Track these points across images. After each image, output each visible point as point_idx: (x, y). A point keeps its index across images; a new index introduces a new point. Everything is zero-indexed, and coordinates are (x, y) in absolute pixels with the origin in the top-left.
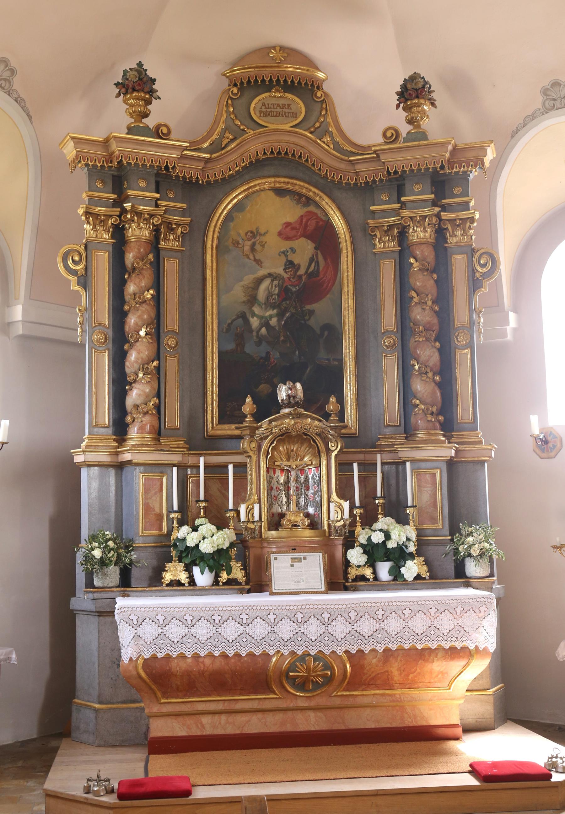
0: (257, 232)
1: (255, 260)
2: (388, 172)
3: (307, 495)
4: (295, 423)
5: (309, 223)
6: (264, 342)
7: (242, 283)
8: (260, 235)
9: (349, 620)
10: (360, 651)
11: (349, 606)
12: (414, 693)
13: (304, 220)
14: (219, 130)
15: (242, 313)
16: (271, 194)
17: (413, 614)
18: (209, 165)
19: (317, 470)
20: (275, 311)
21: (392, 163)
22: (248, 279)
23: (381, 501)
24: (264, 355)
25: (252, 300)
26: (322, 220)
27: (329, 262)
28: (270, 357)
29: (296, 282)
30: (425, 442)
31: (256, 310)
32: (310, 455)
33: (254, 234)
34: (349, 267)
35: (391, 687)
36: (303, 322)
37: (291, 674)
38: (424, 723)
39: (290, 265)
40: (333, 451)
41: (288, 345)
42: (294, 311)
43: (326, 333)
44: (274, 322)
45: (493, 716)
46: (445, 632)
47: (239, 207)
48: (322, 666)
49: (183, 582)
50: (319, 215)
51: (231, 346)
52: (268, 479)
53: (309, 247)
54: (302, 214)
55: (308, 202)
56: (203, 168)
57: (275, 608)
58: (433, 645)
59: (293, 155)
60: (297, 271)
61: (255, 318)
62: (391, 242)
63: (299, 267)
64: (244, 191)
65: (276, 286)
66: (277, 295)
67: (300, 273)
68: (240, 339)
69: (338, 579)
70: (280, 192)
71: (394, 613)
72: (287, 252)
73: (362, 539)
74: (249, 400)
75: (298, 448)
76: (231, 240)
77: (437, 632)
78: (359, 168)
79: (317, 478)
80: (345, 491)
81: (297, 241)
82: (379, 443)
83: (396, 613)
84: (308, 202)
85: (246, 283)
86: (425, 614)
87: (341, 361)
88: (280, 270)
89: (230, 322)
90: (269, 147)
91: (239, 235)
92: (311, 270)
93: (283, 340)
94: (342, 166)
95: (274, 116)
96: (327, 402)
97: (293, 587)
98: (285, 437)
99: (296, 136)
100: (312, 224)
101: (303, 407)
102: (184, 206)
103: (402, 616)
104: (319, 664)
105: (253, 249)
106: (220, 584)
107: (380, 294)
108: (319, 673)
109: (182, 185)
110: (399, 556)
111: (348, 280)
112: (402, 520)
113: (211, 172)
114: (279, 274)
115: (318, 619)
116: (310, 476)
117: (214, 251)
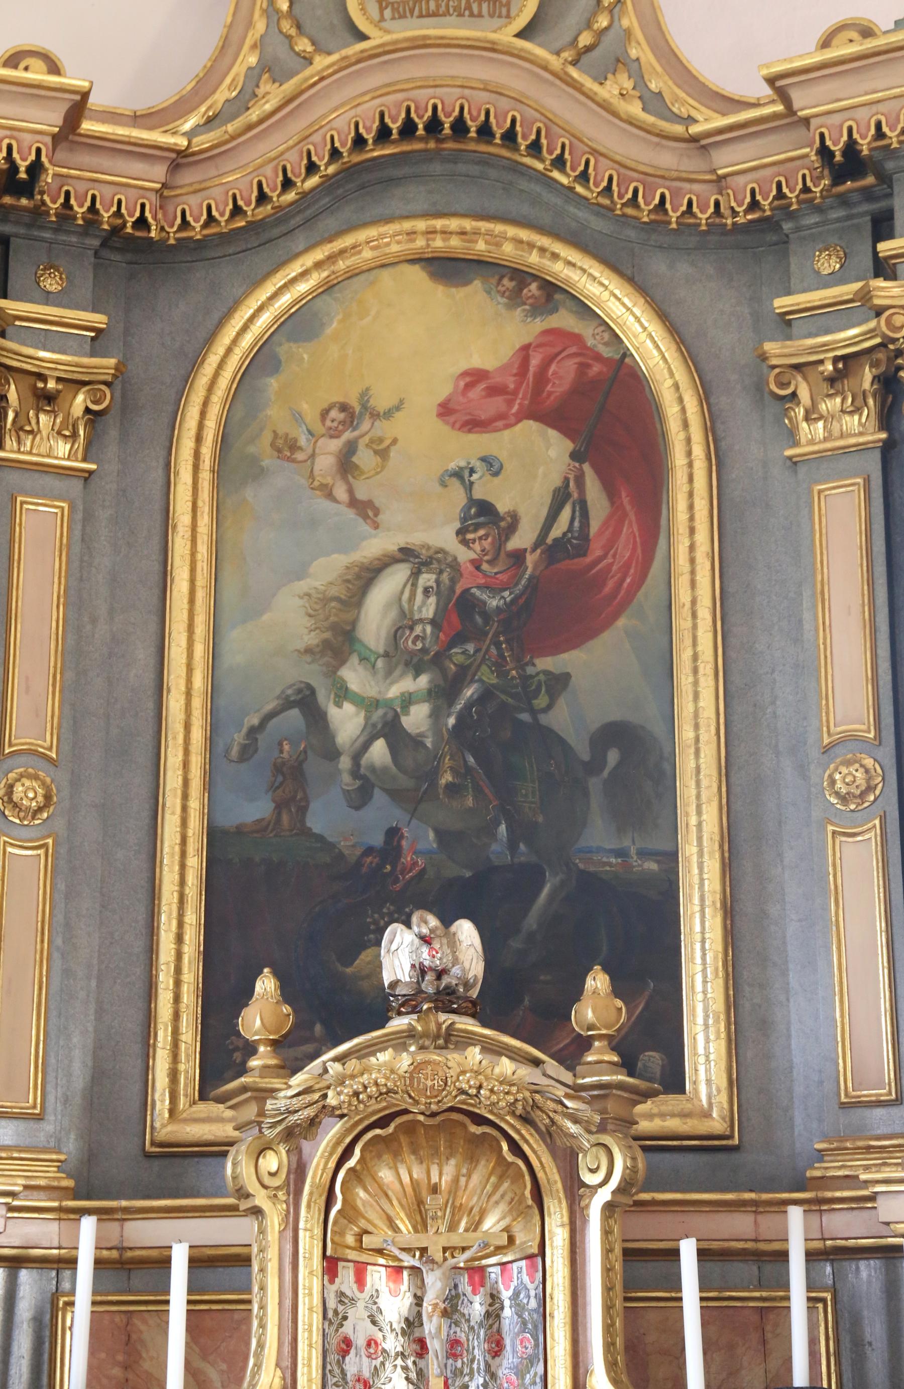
0: (364, 406)
1: (354, 502)
2: (824, 152)
3: (493, 1376)
4: (417, 1067)
5: (553, 367)
6: (377, 792)
7: (303, 586)
8: (375, 416)
13: (535, 362)
14: (239, 70)
15: (300, 691)
16: (416, 274)
18: (188, 177)
20: (424, 681)
21: (836, 119)
22: (327, 571)
24: (377, 840)
25: (340, 642)
26: (598, 357)
27: (626, 500)
28: (399, 848)
29: (503, 577)
31: (354, 676)
32: (503, 1207)
34: (697, 516)
36: (525, 717)
39: (481, 515)
40: (594, 1189)
41: (470, 802)
42: (492, 679)
43: (613, 757)
44: (417, 719)
47: (299, 324)
50: (590, 342)
51: (256, 809)
53: (552, 453)
54: (526, 340)
55: (549, 298)
56: (164, 186)
60: (507, 539)
61: (348, 707)
62: (851, 413)
63: (513, 524)
64: (318, 265)
65: (426, 591)
66: (433, 622)
67: (514, 544)
68: (291, 782)
70: (448, 268)
72: (472, 471)
75: (456, 1180)
76: (267, 437)
78: (728, 160)
79: (533, 1304)
81: (507, 433)
82: (818, 1173)
84: (549, 298)
85: (317, 584)
87: (670, 858)
88: (444, 537)
89: (255, 721)
90: (398, 105)
91: (298, 417)
92: (557, 532)
93: (449, 787)
95: (429, 15)
96: (576, 993)
98: (389, 1128)
99: (492, 60)
100: (564, 374)
101: (474, 1010)
102: (99, 319)
105: (346, 465)
107: (815, 606)
109: (96, 254)
111: (692, 561)
113: (194, 200)
114: (440, 551)
116: (506, 1295)
117: (205, 476)
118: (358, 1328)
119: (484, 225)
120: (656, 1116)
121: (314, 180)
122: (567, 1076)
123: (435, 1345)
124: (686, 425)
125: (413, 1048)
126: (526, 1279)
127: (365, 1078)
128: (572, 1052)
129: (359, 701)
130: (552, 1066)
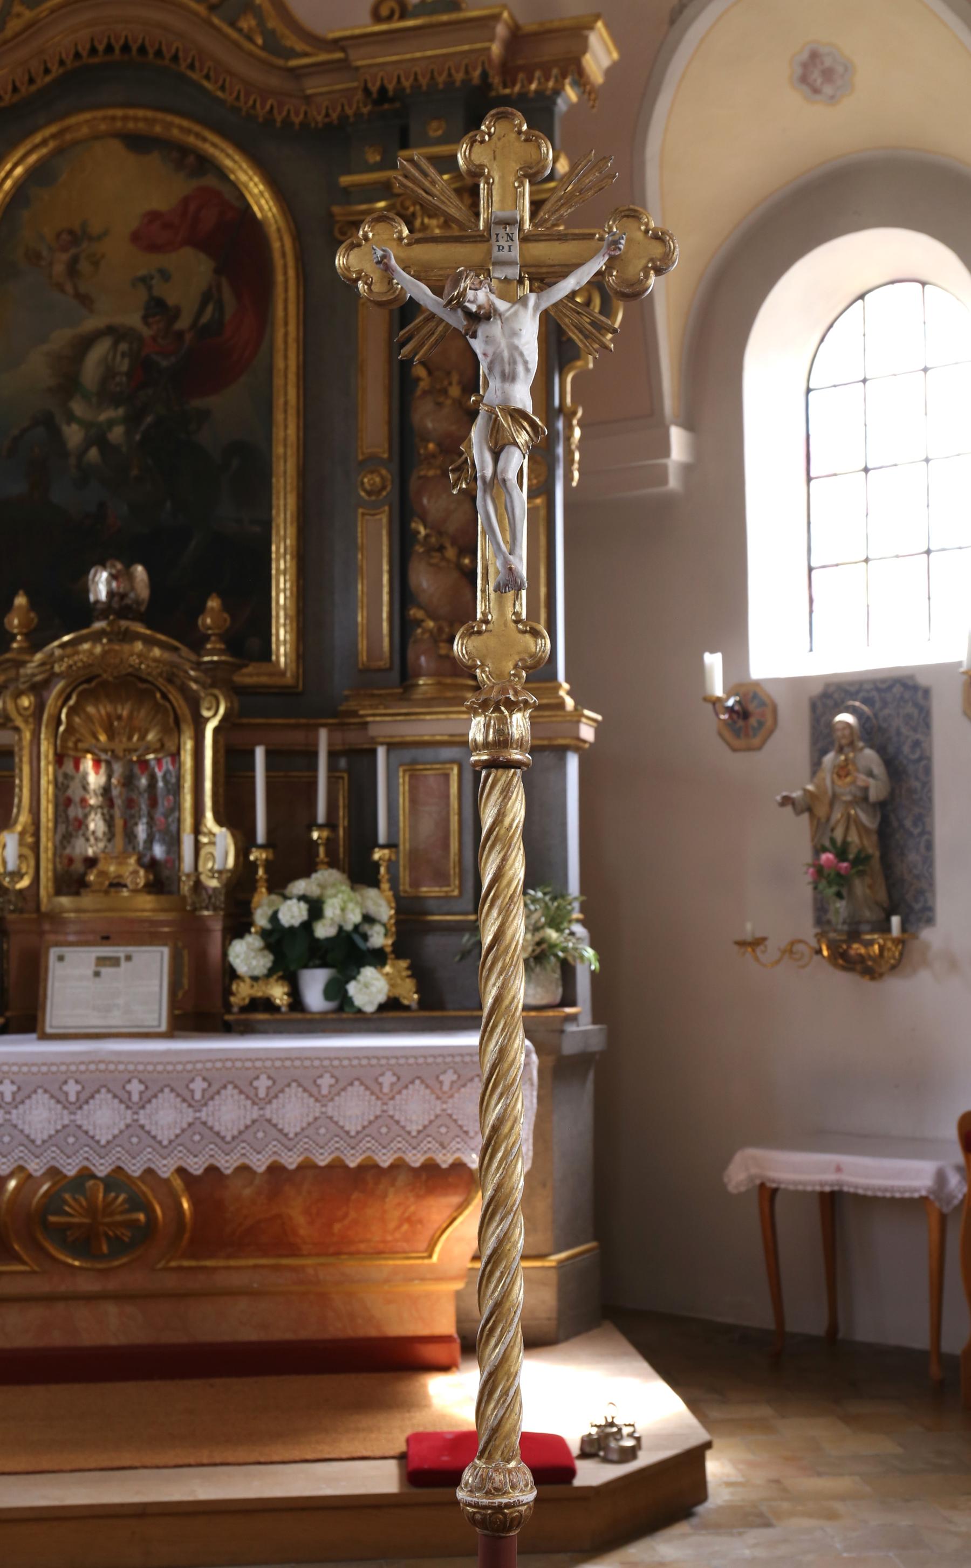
2: (367, 91)
9: (188, 1098)
10: (212, 1170)
11: (189, 1067)
12: (351, 1267)
16: (116, 145)
17: (340, 1088)
19: (173, 763)
20: (121, 411)
22: (61, 338)
23: (325, 834)
30: (428, 702)
33: (76, 237)
35: (294, 1251)
37: (52, 1219)
38: (373, 1333)
39: (157, 308)
44: (117, 434)
45: (554, 1315)
46: (414, 1128)
48: (125, 1201)
49: (406, 1002)
52: (60, 779)
57: (15, 1069)
58: (384, 1158)
59: (159, 53)
64: (53, 136)
69: (204, 1005)
70: (138, 143)
71: (294, 1085)
72: (152, 278)
73: (261, 919)
74: (21, 600)
77: (395, 1128)
78: (314, 86)
80: (234, 813)
83: (300, 1085)
86: (367, 1088)
88: (134, 320)
94: (274, 81)
96: (201, 609)
97: (94, 1021)
103: (314, 1090)
104: (116, 1198)
105: (72, 270)
106: (235, 1009)
108: (119, 1218)
110: (348, 954)
112: (362, 875)
115: (115, 1096)
116: (159, 774)
118: (74, 791)
119: (160, 115)
120: (250, 675)
121: (48, 79)
122: (193, 657)
123: (118, 802)
124: (284, 255)
125: (105, 641)
126: (171, 767)
127: (76, 658)
128: (197, 643)
129: (81, 422)
130: (185, 651)
